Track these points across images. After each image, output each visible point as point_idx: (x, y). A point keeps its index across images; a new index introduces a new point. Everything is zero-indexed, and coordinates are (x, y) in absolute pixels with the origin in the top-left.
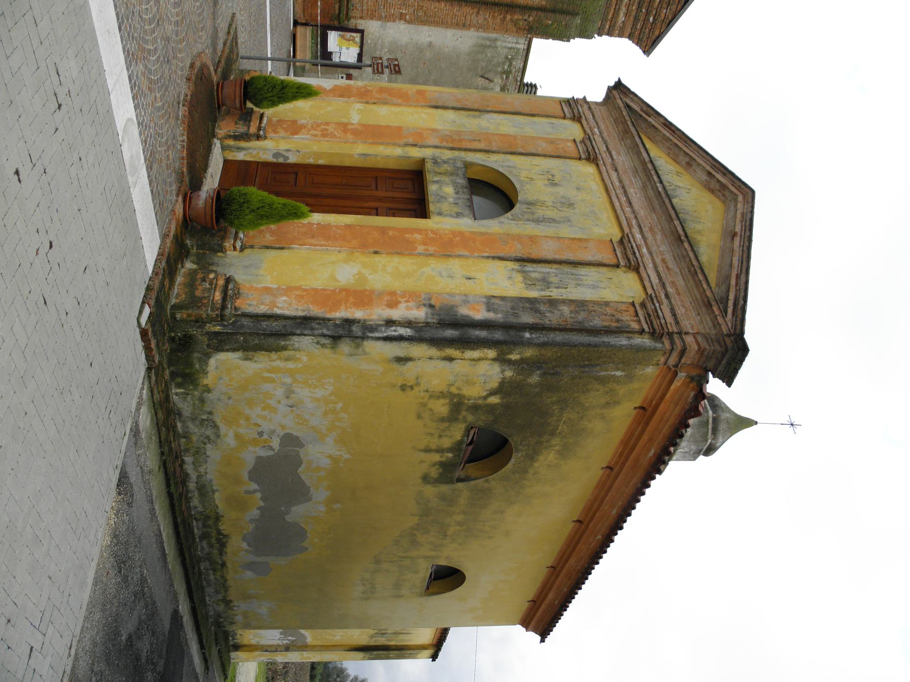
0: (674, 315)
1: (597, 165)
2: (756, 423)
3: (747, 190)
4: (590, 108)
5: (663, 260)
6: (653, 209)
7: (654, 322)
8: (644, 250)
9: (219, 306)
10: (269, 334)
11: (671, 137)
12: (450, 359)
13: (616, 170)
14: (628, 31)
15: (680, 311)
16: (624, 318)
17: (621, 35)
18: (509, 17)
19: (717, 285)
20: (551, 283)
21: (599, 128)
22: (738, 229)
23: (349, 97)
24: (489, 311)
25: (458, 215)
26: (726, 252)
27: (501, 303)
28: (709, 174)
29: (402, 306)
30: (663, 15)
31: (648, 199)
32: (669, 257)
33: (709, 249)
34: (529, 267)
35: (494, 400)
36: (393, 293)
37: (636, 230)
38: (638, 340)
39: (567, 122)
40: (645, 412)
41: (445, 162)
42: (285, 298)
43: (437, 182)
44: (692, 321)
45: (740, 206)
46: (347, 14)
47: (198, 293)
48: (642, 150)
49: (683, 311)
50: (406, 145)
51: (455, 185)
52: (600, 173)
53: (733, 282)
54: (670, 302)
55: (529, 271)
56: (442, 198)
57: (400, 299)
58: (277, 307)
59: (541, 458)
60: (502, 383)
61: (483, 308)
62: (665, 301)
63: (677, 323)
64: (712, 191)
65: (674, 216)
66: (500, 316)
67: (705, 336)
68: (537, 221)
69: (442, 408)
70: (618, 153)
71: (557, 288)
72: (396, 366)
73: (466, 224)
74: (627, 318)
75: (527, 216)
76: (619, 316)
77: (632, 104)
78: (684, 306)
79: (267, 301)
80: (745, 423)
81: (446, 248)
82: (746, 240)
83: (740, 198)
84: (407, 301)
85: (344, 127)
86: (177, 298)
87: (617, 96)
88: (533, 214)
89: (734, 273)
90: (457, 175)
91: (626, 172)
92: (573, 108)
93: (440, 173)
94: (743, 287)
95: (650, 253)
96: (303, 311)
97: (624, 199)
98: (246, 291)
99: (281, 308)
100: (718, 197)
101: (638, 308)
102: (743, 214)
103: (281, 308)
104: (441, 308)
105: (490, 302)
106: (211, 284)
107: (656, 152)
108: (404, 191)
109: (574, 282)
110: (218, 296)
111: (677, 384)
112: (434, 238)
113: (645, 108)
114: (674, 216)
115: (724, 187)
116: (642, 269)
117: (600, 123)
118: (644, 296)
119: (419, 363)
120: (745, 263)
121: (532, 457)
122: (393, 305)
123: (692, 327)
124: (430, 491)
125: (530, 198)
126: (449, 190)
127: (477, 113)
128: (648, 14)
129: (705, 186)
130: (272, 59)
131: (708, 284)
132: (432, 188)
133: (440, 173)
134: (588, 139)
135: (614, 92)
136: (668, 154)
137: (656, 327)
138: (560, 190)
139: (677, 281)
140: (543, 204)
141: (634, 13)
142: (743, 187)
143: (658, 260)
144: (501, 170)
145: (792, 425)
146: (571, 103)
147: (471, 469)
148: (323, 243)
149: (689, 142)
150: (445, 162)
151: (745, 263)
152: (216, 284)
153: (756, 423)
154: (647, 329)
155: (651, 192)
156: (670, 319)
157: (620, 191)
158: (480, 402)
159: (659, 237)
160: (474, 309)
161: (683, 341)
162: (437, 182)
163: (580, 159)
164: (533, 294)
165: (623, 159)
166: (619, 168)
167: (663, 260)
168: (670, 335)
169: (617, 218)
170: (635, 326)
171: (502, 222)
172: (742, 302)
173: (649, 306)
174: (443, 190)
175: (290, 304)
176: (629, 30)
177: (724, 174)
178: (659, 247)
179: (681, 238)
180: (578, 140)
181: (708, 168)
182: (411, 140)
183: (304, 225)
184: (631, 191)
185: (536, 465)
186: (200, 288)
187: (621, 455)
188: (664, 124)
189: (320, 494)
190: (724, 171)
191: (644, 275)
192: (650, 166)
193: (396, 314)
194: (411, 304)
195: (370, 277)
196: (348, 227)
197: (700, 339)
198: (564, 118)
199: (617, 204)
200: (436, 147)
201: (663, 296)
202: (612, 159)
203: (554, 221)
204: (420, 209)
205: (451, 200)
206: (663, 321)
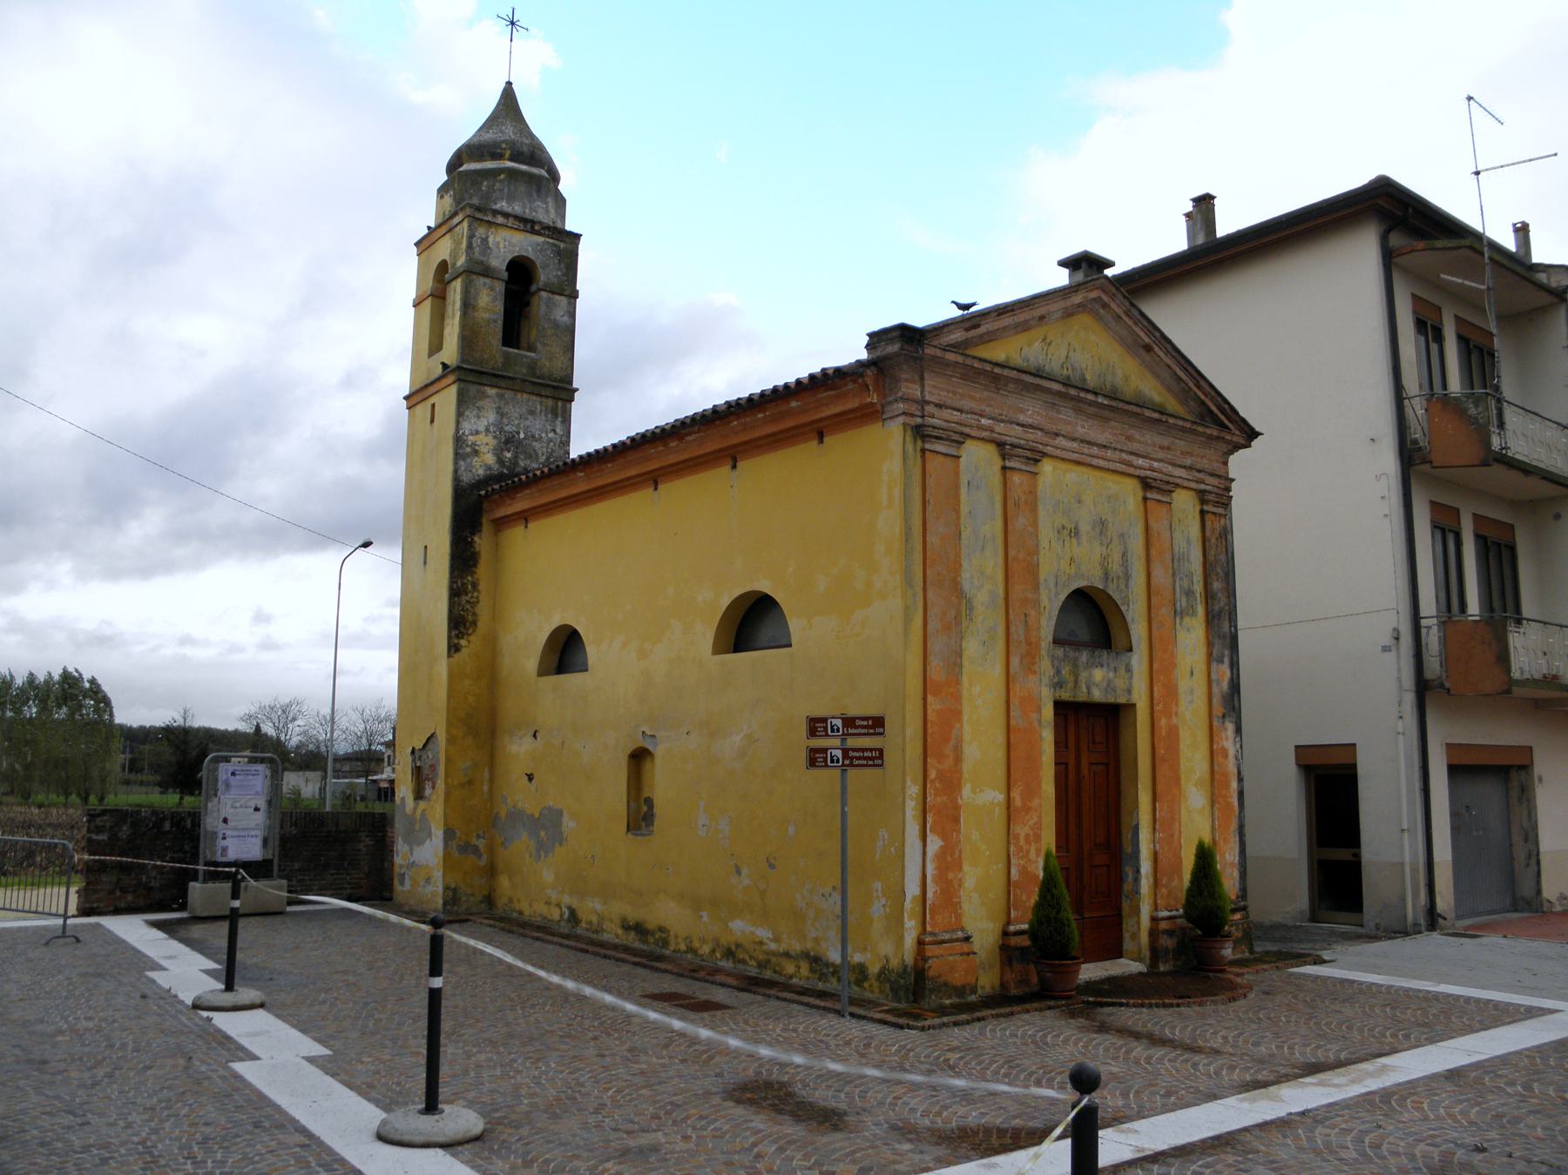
2: (509, 83)
5: (1162, 448)
13: (1057, 435)
23: (957, 808)
25: (1129, 670)
41: (1058, 672)
43: (1088, 688)
51: (1090, 665)
56: (1110, 686)
68: (1127, 577)
73: (1139, 660)
75: (1122, 587)
80: (508, 102)
90: (1076, 659)
93: (1076, 682)
97: (1095, 450)
107: (998, 352)
113: (967, 325)
125: (1099, 573)
126: (1098, 674)
132: (1097, 696)
133: (1076, 682)
138: (1084, 528)
140: (1104, 559)
150: (1058, 672)
153: (509, 83)
155: (1091, 410)
162: (1088, 688)
169: (1114, 471)
174: (1096, 681)
183: (201, 1018)
192: (1073, 392)
199: (1101, 463)
203: (1124, 554)
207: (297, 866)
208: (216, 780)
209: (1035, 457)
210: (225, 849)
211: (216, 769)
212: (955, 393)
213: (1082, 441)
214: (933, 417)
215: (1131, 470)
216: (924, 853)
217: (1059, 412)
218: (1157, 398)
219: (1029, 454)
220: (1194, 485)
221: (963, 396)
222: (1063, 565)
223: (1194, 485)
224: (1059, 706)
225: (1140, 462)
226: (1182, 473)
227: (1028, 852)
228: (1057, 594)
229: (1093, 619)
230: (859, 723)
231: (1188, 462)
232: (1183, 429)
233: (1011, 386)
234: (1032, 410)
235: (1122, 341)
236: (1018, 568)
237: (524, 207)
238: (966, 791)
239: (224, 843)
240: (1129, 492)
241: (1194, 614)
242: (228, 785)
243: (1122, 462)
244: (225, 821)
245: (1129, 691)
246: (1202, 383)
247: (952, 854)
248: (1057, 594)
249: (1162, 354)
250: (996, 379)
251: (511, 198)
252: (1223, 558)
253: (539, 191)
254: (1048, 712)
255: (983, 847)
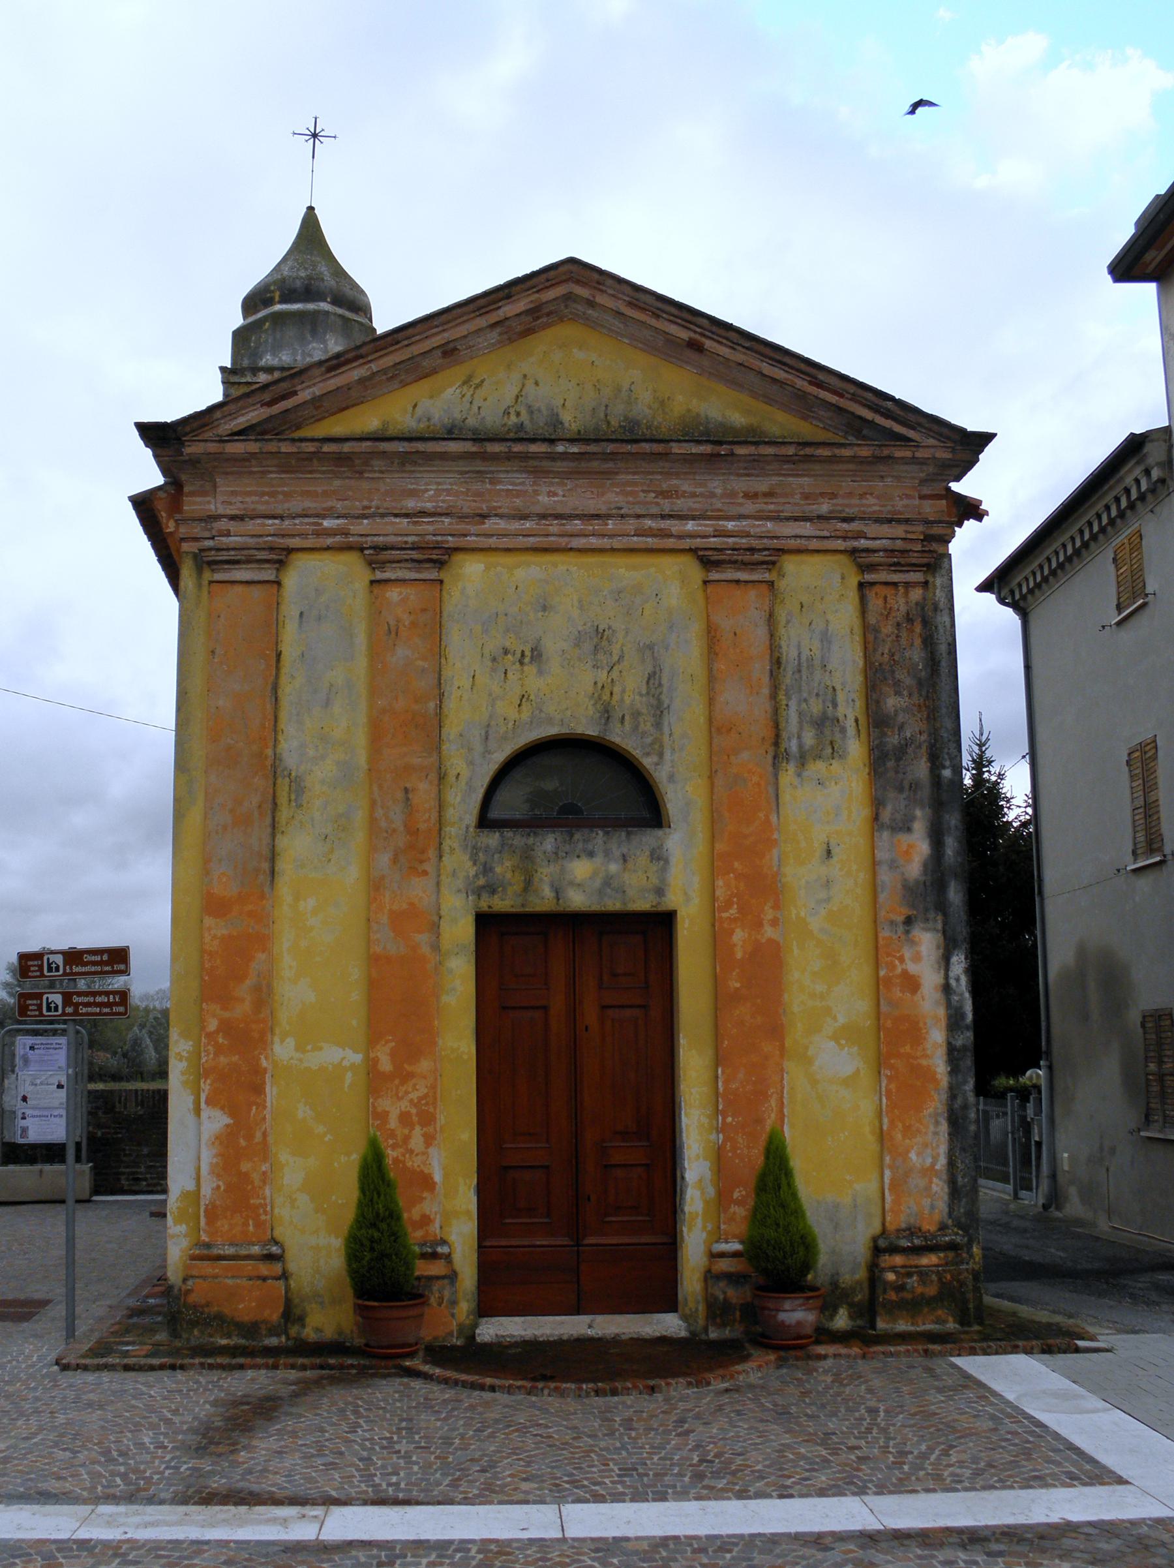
1: (457, 550)
2: (311, 209)
3: (561, 269)
5: (751, 496)
7: (914, 561)
9: (951, 1254)
11: (374, 367)
13: (484, 516)
16: (903, 609)
20: (824, 713)
24: (909, 830)
27: (889, 808)
29: (912, 968)
32: (740, 485)
41: (487, 869)
42: (913, 1155)
47: (932, 1291)
49: (871, 500)
55: (800, 746)
57: (899, 970)
58: (933, 1165)
61: (904, 839)
66: (918, 813)
71: (835, 705)
76: (900, 615)
78: (862, 496)
79: (922, 1183)
80: (311, 232)
82: (695, 319)
84: (902, 960)
86: (945, 1322)
88: (636, 714)
91: (479, 494)
96: (937, 1123)
98: (903, 1218)
99: (935, 1159)
100: (547, 326)
103: (935, 1159)
104: (913, 906)
106: (909, 1275)
109: (818, 674)
110: (928, 1260)
120: (787, 360)
126: (580, 868)
129: (511, 341)
130: (578, 1251)
136: (404, 384)
137: (925, 561)
138: (553, 646)
142: (552, 273)
148: (773, 1103)
149: (400, 335)
150: (487, 869)
151: (787, 360)
152: (903, 1267)
153: (311, 209)
155: (559, 466)
157: (554, 527)
160: (907, 853)
171: (671, 778)
172: (889, 404)
174: (583, 876)
175: (925, 1145)
177: (509, 297)
186: (919, 1290)
188: (330, 370)
190: (501, 294)
191: (793, 543)
194: (907, 953)
195: (842, 1020)
197: (926, 491)
199: (594, 542)
201: (845, 526)
203: (653, 677)
205: (613, 868)
207: (145, 1151)
208: (14, 1055)
209: (436, 557)
210: (25, 1130)
211: (13, 1044)
212: (272, 494)
213: (543, 516)
214: (228, 535)
215: (670, 543)
216: (199, 1135)
217: (493, 482)
218: (737, 419)
219: (415, 555)
220: (840, 544)
221: (288, 495)
222: (486, 714)
223: (840, 544)
224: (485, 922)
225: (690, 526)
226: (806, 529)
227: (406, 1139)
228: (487, 752)
229: (584, 780)
230: (87, 958)
231: (824, 508)
232: (787, 459)
233: (377, 463)
234: (434, 489)
235: (650, 348)
236: (409, 723)
237: (294, 354)
238: (283, 1050)
239: (23, 1123)
240: (672, 583)
241: (836, 752)
242: (26, 1061)
243: (650, 533)
244: (24, 1099)
245: (660, 892)
246: (821, 376)
247: (250, 1137)
248: (487, 752)
249: (724, 351)
250: (342, 460)
251: (276, 349)
252: (916, 655)
253: (314, 332)
254: (460, 930)
255: (321, 1129)
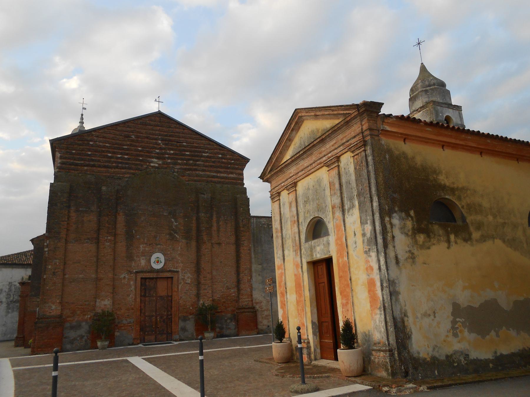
0: (355, 137)
2: (422, 63)
4: (274, 189)
6: (312, 154)
8: (330, 155)
10: (399, 328)
12: (393, 237)
13: (298, 173)
14: (239, 171)
15: (353, 134)
17: (242, 174)
18: (242, 229)
19: (339, 119)
21: (281, 184)
22: (313, 114)
26: (324, 117)
28: (292, 130)
30: (230, 157)
31: (308, 157)
32: (332, 143)
33: (327, 124)
34: (346, 207)
35: (412, 213)
36: (367, 269)
37: (322, 160)
38: (369, 152)
39: (281, 198)
40: (405, 138)
44: (356, 128)
45: (303, 115)
46: (251, 308)
48: (287, 163)
50: (302, 271)
52: (300, 180)
53: (335, 112)
54: (350, 139)
59: (443, 183)
60: (401, 211)
62: (350, 142)
63: (358, 135)
64: (299, 128)
65: (312, 144)
67: (361, 121)
69: (421, 238)
70: (291, 173)
72: (401, 264)
73: (332, 238)
74: (359, 158)
77: (269, 170)
81: (344, 247)
83: (300, 115)
85: (298, 302)
87: (266, 177)
89: (331, 112)
92: (275, 196)
94: (337, 108)
95: (330, 152)
101: (355, 154)
102: (306, 113)
105: (363, 223)
107: (288, 156)
108: (323, 270)
111: (388, 128)
112: (339, 252)
114: (312, 144)
115: (296, 123)
116: (338, 155)
117: (279, 183)
118: (349, 152)
119: (398, 252)
121: (443, 188)
122: (372, 268)
123: (359, 127)
124: (476, 235)
127: (284, 240)
128: (231, 164)
131: (338, 124)
134: (287, 188)
135: (265, 179)
139: (341, 138)
141: (231, 170)
143: (333, 148)
144: (306, 226)
145: (419, 44)
146: (272, 197)
147: (457, 215)
153: (422, 63)
154: (363, 149)
155: (305, 156)
156: (357, 139)
157: (306, 170)
158: (415, 219)
159: (323, 149)
161: (365, 131)
163: (296, 190)
164: (356, 203)
165: (293, 170)
166: (297, 172)
167: (333, 146)
168: (363, 137)
170: (363, 154)
173: (353, 149)
176: (239, 171)
178: (327, 149)
179: (322, 139)
180: (288, 192)
181: (290, 131)
182: (300, 270)
184: (306, 165)
185: (448, 184)
187: (434, 143)
189: (489, 294)
192: (293, 159)
193: (376, 267)
196: (341, 294)
198: (279, 200)
199: (312, 170)
200: (301, 257)
202: (294, 175)
204: (328, 261)
206: (359, 142)
